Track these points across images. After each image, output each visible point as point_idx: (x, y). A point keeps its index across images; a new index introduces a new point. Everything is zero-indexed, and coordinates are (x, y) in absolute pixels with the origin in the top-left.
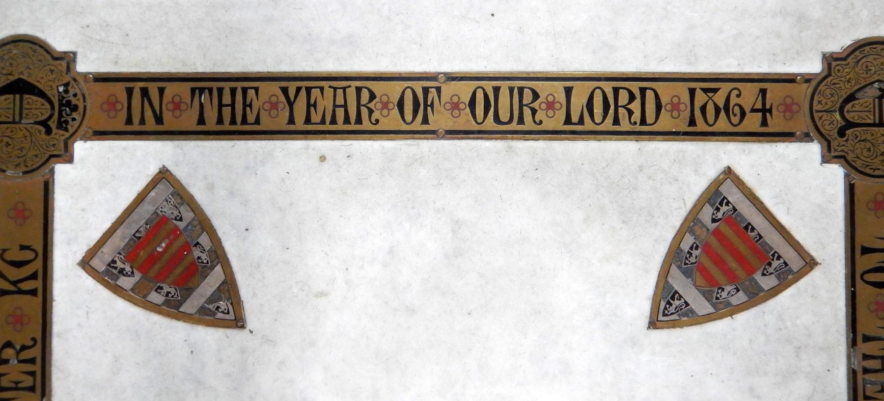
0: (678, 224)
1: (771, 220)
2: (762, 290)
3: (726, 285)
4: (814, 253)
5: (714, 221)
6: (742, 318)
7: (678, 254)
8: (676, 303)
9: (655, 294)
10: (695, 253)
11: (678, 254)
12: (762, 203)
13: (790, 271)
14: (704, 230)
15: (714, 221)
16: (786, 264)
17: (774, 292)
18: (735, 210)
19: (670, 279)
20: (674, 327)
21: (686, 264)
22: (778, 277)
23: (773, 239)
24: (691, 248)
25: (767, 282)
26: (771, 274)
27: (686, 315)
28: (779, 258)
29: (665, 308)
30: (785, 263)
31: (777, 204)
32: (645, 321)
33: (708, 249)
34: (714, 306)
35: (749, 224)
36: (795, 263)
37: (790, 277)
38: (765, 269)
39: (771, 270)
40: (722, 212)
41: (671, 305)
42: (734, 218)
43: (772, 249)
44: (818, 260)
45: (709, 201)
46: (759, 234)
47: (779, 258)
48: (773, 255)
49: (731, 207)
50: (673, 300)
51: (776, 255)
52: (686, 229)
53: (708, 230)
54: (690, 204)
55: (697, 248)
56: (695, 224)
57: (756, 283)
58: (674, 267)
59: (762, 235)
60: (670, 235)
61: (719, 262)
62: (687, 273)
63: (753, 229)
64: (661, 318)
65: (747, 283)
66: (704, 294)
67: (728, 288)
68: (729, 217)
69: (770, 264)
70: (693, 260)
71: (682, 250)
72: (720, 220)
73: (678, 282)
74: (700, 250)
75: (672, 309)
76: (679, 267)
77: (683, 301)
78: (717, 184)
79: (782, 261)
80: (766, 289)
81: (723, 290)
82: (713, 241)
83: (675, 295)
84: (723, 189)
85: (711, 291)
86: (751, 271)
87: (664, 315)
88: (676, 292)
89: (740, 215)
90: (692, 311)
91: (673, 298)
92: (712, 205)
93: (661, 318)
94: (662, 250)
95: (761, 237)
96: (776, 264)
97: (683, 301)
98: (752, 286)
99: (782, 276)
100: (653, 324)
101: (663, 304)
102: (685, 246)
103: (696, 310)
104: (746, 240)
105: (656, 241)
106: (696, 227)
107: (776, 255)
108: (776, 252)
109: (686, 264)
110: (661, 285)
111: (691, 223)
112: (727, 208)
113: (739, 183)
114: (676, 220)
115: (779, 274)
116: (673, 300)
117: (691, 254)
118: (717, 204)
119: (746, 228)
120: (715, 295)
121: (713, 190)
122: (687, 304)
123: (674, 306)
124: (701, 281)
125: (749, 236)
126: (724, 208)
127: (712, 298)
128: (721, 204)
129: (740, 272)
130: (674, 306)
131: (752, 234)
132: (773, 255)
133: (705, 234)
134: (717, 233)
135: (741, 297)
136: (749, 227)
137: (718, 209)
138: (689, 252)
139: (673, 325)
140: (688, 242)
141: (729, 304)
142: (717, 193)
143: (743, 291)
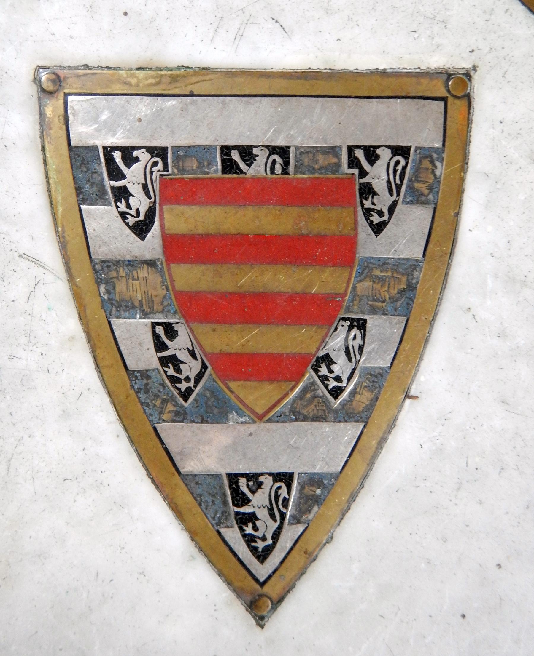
0: (73, 325)
1: (263, 87)
2: (413, 266)
3: (323, 342)
4: (436, 61)
5: (141, 229)
6: (434, 373)
7: (146, 389)
8: (258, 502)
9: (194, 535)
10: (178, 347)
11: (146, 389)
12: (205, 71)
13: (429, 156)
14: (143, 272)
15: (141, 229)
16: (402, 151)
17: (442, 240)
18: (159, 152)
19: (189, 467)
20: (311, 558)
21: (186, 395)
22: (417, 199)
23: (312, 126)
24: (160, 346)
25: (405, 236)
26: (392, 209)
27: (309, 502)
28: (371, 154)
29: (249, 540)
30: (278, 477)
31: (239, 36)
32: (236, 613)
33: (199, 308)
34: (346, 415)
35: (226, 150)
36: (420, 128)
37: (440, 170)
38: (367, 213)
39: (383, 200)
40: (136, 190)
41: (252, 518)
42: (185, 177)
43: (333, 150)
44: (462, 64)
45: (83, 198)
46: (273, 150)
47: (371, 154)
48: (353, 162)
49: (144, 157)
50: (246, 501)
51: (360, 154)
52: (101, 315)
53: (151, 263)
54: (49, 253)
55: (171, 332)
56: (110, 283)
57: (383, 264)
58: (167, 430)
59: (280, 142)
60: (81, 369)
61: (253, 308)
62: (215, 411)
63: (247, 153)
64: (262, 571)
65: (364, 287)
66: (297, 415)
67: (336, 343)
68: (165, 182)
69: (367, 191)
70: (190, 368)
71: (145, 374)
72: (151, 213)
73: (211, 449)
74: (182, 329)
75: (266, 526)
76: (181, 416)
77: (267, 481)
78: (54, 128)
79: (385, 154)
80: (418, 253)
81: (328, 360)
82: (191, 276)
83: (237, 487)
84: (83, 133)
85: (305, 390)
86: (341, 251)
87: (262, 556)
88: (233, 478)
89: (185, 152)
90: (315, 480)
91: (241, 500)
92: (99, 198)
93: (262, 571)
94: (101, 417)
95: (283, 152)
96: (378, 175)
97: (267, 481)
98: (381, 280)
99: (422, 187)
100: (259, 601)
101: (233, 535)
102: (142, 355)
103: (318, 469)
104: (259, 194)
105: (65, 414)
106: (121, 287)
107: (360, 154)
108: (351, 150)
109: (186, 395)
110: (185, 498)
111: (102, 291)
112: (137, 167)
113: (106, 81)
114: (60, 320)
115: (411, 189)
116: (246, 501)
117: (173, 361)
118: (109, 184)
119: (229, 166)
120: (322, 391)
121: (60, 160)
122: (286, 478)
123: (262, 514)
124: (258, 394)
125: (256, 180)
126: (133, 177)
127: (325, 402)
128: (115, 173)
129: (321, 280)
130: (262, 514)
131: (258, 168)
132: (353, 162)
133: (154, 278)
134: (177, 248)
135: (383, 329)
136: (234, 158)
137: (122, 194)
138: (164, 362)
139: (305, 555)
140: (135, 334)
141: (376, 379)
142: (80, 156)
143: (374, 311)
